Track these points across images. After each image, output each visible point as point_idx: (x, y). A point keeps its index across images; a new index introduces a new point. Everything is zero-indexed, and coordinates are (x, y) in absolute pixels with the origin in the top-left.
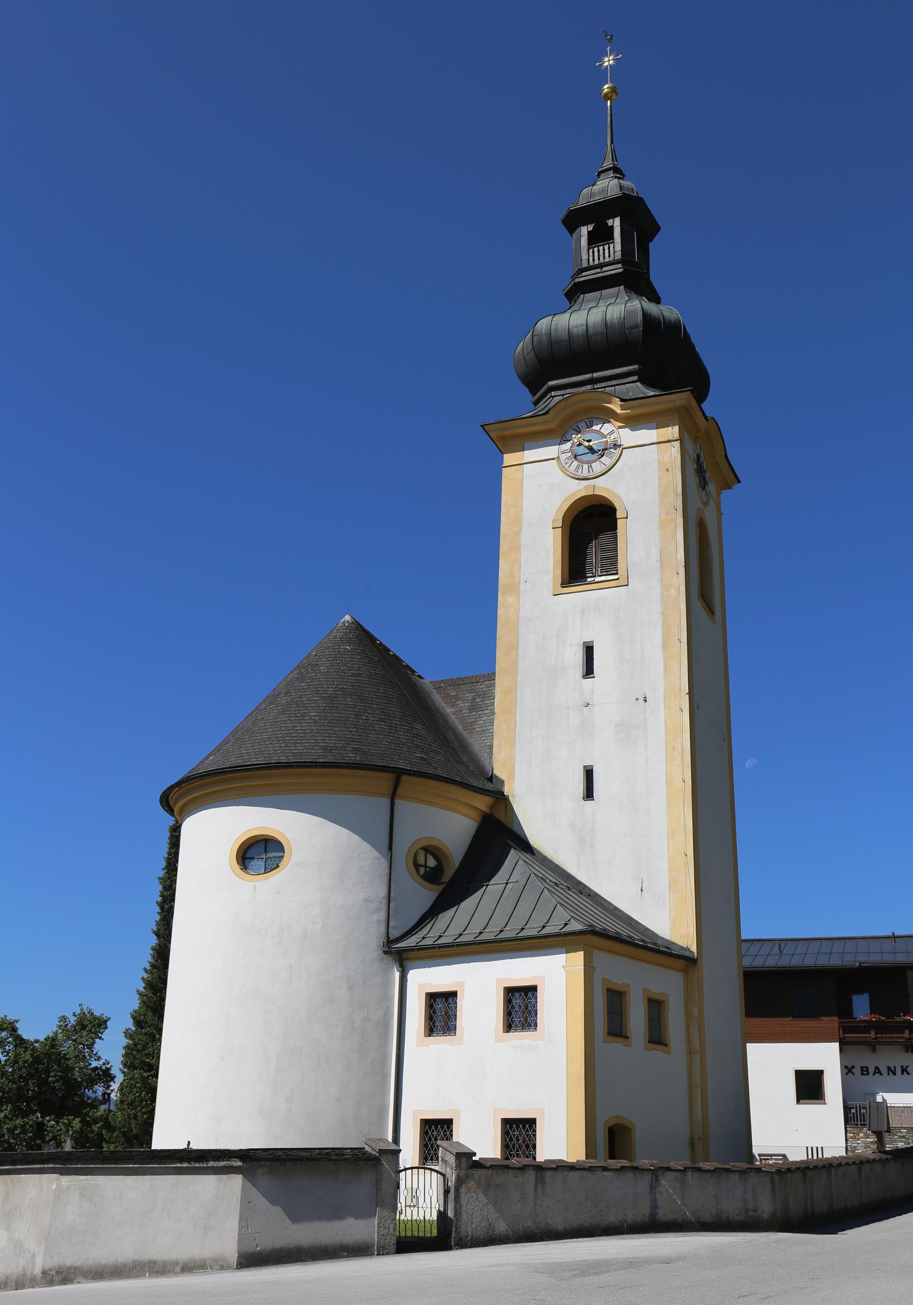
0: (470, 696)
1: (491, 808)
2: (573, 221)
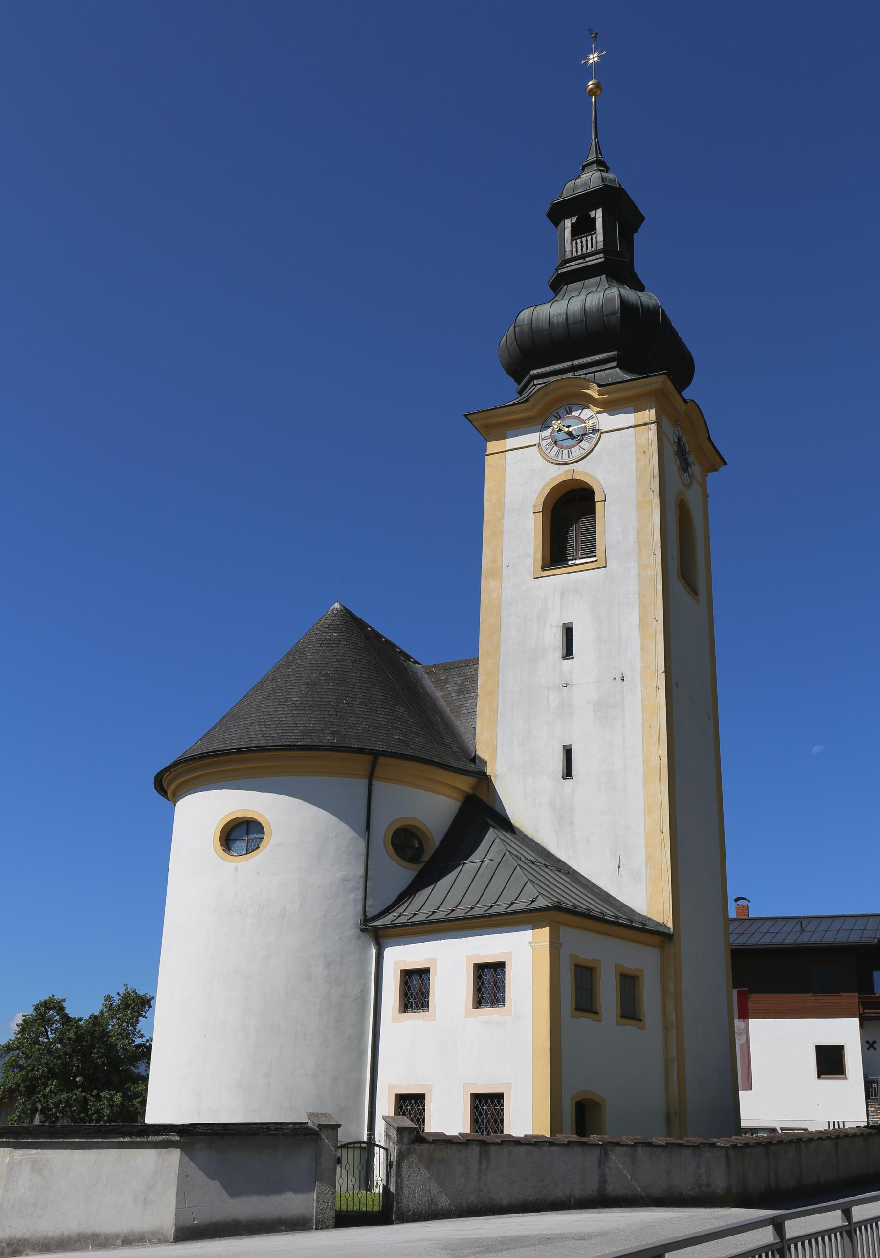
0: (458, 679)
1: (474, 788)
2: (557, 214)
